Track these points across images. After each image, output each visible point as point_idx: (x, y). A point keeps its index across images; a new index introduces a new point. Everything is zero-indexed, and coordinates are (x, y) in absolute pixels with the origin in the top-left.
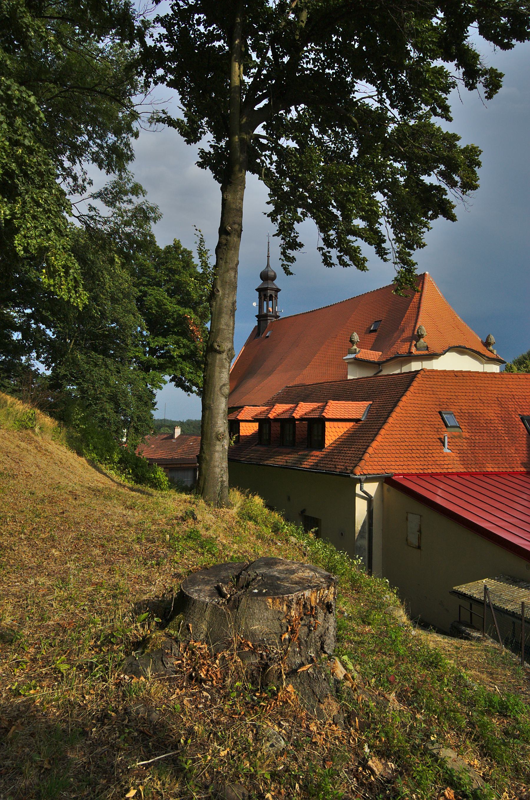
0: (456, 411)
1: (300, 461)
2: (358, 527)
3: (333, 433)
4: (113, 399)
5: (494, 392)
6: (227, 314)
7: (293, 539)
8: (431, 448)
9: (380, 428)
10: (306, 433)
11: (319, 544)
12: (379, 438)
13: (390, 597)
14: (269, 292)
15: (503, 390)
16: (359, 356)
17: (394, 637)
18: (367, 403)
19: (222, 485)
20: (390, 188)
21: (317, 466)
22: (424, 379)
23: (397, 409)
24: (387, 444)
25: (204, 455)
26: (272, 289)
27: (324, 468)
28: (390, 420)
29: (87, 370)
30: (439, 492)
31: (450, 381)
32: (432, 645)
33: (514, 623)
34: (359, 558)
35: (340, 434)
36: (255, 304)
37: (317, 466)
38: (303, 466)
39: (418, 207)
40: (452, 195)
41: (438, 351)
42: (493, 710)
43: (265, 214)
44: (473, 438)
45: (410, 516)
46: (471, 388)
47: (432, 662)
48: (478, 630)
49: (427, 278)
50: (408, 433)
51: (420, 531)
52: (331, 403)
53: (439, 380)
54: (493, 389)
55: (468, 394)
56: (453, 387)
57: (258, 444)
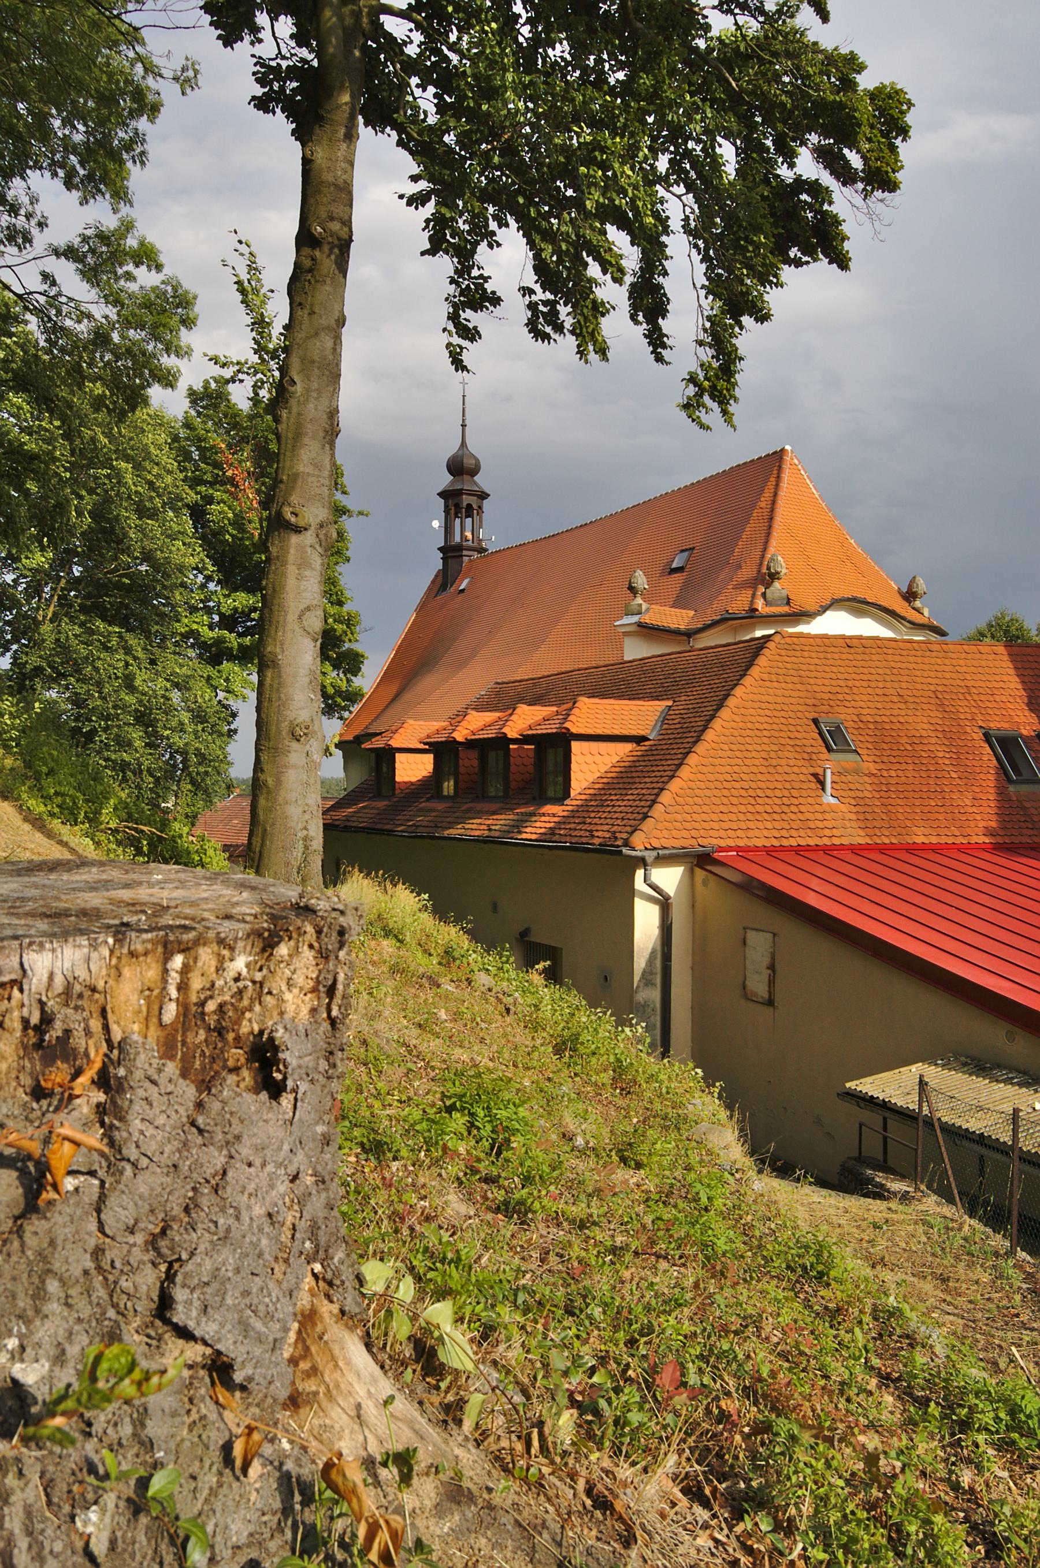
0: (849, 718)
1: (518, 826)
2: (640, 963)
3: (589, 767)
4: (144, 719)
5: (929, 680)
6: (313, 438)
7: (483, 979)
8: (795, 793)
9: (688, 753)
10: (531, 769)
11: (547, 993)
12: (684, 772)
13: (706, 1106)
14: (466, 500)
15: (947, 676)
16: (647, 619)
17: (704, 1200)
18: (661, 705)
19: (306, 847)
20: (703, 179)
21: (554, 834)
22: (783, 653)
23: (725, 713)
24: (702, 785)
25: (262, 777)
26: (472, 493)
27: (568, 839)
28: (709, 735)
29: (87, 658)
30: (814, 883)
31: (836, 656)
32: (802, 1215)
33: (982, 1159)
34: (637, 1024)
35: (603, 769)
36: (436, 524)
37: (554, 834)
38: (524, 836)
39: (767, 233)
40: (844, 202)
41: (811, 607)
42: (1023, 1443)
43: (401, 197)
44: (885, 774)
45: (751, 935)
46: (880, 671)
47: (810, 1271)
48: (903, 1176)
49: (787, 458)
50: (747, 762)
51: (772, 967)
52: (584, 702)
53: (814, 655)
54: (925, 674)
55: (873, 684)
56: (842, 670)
57: (432, 797)
